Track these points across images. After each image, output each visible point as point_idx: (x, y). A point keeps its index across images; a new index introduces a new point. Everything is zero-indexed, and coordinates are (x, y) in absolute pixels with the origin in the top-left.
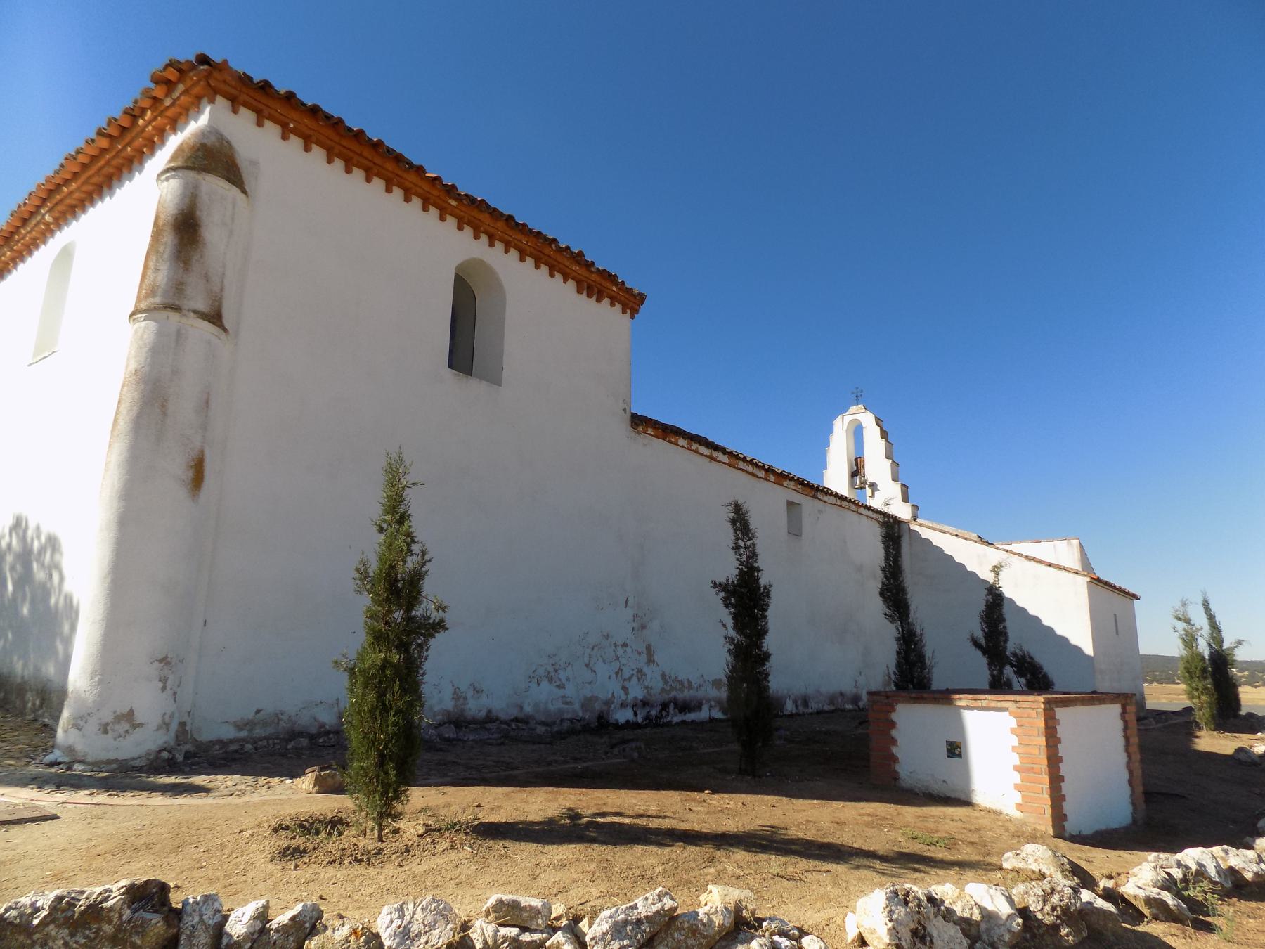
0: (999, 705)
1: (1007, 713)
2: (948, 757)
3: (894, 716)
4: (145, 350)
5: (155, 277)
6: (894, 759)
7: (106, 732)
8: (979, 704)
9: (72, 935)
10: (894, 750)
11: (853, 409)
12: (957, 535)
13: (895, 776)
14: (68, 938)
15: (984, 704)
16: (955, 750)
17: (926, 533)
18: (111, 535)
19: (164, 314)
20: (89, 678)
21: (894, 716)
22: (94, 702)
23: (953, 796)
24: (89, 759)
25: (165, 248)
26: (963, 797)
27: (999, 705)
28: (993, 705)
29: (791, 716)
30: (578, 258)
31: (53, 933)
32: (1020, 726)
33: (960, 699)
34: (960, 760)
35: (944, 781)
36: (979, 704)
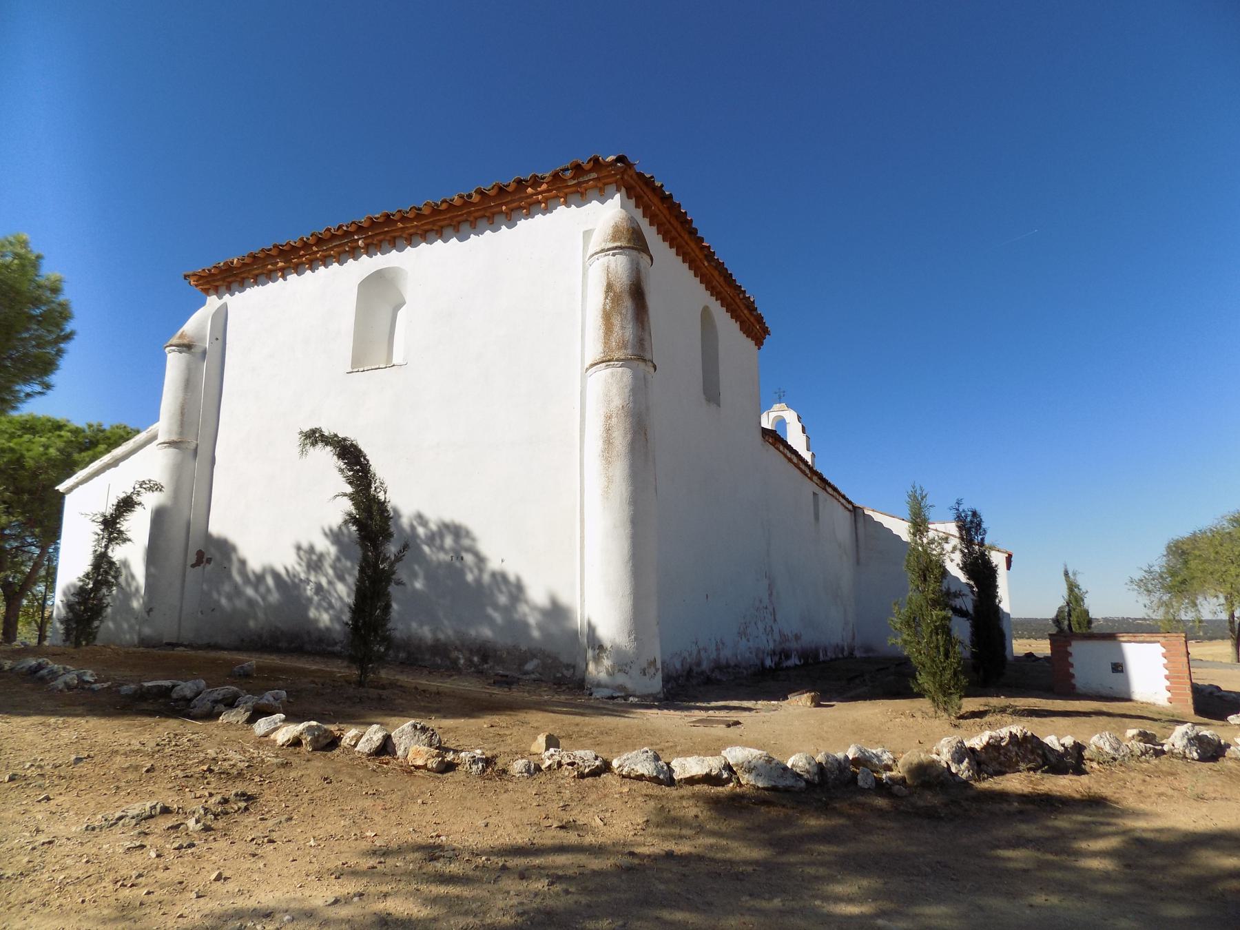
0: (1152, 639)
1: (1159, 644)
2: (1113, 672)
3: (1070, 649)
4: (627, 390)
5: (623, 333)
6: (1072, 676)
7: (645, 674)
8: (1138, 639)
9: (1019, 749)
10: (1071, 670)
11: (776, 406)
12: (903, 520)
13: (1074, 687)
14: (1018, 751)
15: (1141, 639)
16: (1119, 668)
17: (878, 517)
18: (627, 531)
19: (636, 363)
20: (627, 636)
21: (1070, 649)
22: (634, 653)
23: (1118, 696)
24: (638, 693)
25: (627, 311)
26: (1126, 696)
27: (1152, 639)
28: (1148, 639)
29: (824, 662)
30: (751, 307)
31: (1011, 748)
32: (1168, 651)
33: (1123, 636)
34: (1121, 674)
35: (1111, 688)
36: (1138, 639)
